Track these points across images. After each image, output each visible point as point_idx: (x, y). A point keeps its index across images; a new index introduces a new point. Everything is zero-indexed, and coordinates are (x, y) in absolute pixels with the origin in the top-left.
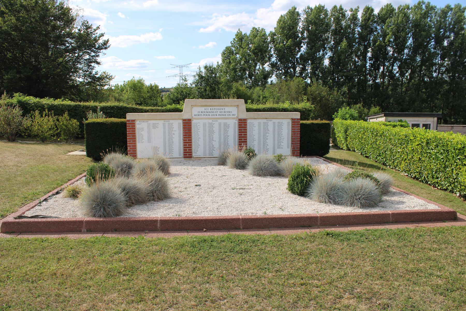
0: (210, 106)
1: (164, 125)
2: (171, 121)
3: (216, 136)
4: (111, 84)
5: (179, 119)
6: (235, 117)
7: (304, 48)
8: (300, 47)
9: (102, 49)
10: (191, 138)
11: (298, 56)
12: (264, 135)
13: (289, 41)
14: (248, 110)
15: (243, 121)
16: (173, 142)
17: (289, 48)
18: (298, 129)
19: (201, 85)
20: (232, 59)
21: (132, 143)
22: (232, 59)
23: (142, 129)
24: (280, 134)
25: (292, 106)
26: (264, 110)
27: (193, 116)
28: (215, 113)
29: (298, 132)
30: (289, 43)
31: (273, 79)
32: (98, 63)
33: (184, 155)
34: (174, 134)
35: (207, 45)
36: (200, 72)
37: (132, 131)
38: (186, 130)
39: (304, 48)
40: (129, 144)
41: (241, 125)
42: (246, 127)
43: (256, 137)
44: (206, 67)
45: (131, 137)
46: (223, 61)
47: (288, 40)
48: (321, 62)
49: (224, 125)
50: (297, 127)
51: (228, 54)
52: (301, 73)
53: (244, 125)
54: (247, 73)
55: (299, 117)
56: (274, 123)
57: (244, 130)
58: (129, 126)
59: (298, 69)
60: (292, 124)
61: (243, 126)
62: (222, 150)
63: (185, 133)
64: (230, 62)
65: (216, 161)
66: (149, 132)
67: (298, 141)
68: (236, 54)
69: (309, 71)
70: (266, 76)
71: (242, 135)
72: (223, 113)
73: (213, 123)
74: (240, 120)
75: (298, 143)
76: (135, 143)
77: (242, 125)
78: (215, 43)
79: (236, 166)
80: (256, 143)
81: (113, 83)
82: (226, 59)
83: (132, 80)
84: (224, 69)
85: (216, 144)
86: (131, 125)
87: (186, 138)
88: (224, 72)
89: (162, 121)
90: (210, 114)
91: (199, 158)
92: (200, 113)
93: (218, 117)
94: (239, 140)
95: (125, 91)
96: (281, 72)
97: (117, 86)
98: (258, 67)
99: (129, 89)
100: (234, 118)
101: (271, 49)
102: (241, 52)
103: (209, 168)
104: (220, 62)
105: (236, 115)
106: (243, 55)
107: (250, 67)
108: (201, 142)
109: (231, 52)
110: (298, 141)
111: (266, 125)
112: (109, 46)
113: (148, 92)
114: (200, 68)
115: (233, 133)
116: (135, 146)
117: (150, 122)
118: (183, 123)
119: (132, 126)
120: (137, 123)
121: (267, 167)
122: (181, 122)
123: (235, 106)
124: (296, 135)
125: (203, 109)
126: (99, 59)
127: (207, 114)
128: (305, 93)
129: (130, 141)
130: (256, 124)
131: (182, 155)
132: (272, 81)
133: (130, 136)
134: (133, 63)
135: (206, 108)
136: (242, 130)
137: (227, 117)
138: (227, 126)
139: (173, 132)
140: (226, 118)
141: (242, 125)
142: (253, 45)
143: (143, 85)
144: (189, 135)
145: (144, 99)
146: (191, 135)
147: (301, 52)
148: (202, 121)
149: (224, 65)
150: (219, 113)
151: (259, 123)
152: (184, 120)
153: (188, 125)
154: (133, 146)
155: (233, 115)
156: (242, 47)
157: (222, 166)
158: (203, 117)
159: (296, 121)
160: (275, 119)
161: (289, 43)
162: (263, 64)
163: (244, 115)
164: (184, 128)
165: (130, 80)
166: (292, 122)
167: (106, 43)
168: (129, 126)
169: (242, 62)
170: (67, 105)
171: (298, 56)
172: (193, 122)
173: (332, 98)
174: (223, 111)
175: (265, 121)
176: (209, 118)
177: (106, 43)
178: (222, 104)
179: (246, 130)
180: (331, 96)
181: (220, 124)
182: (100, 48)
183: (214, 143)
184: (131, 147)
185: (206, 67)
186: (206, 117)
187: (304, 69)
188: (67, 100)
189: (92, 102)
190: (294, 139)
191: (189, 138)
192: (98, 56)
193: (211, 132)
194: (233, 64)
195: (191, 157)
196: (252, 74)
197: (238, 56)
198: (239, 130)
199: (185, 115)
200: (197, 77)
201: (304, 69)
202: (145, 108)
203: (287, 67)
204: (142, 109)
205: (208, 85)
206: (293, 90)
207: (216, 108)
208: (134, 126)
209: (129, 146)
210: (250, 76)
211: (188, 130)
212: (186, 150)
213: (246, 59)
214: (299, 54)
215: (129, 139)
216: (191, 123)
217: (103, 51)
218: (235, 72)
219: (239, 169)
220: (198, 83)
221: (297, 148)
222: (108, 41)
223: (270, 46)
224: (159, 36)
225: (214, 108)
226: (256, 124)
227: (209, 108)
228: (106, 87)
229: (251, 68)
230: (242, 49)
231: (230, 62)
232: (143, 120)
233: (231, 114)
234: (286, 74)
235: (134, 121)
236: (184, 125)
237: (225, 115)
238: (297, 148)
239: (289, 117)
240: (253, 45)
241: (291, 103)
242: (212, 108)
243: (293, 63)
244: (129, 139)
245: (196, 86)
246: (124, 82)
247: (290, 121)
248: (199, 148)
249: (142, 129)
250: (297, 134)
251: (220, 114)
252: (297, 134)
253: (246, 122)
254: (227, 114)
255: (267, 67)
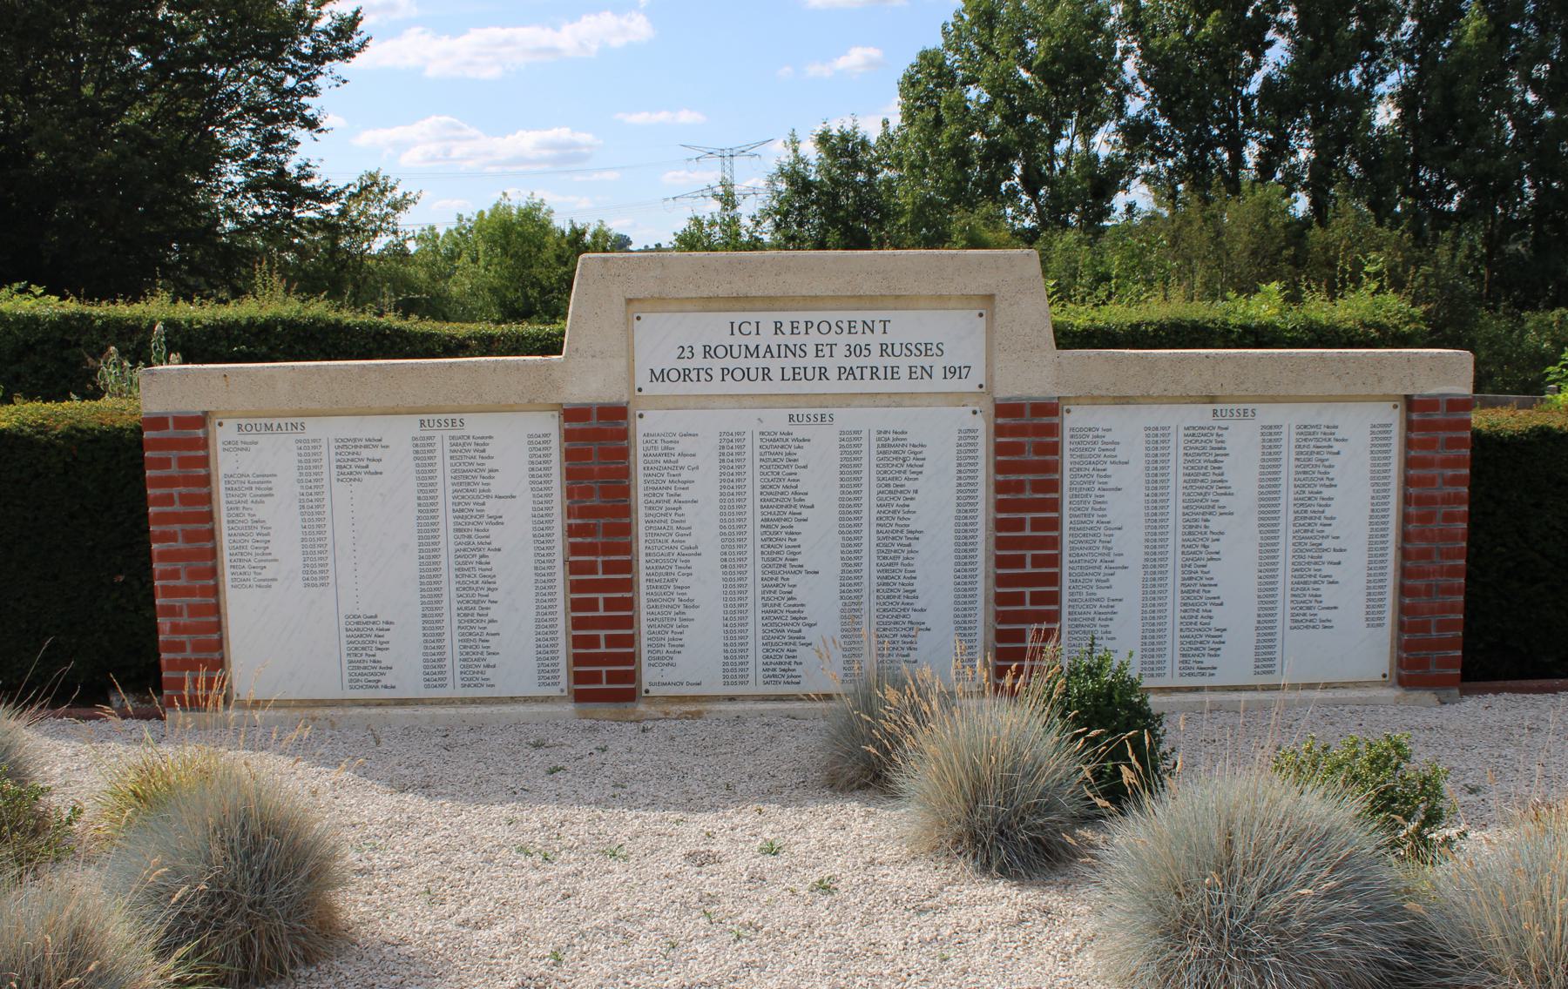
0: (770, 302)
1: (423, 452)
2: (475, 425)
3: (819, 540)
4: (400, 228)
5: (532, 406)
6: (969, 384)
7: (1279, 53)
8: (1260, 48)
9: (330, 57)
10: (627, 548)
11: (1254, 87)
12: (1190, 530)
13: (1210, 20)
14: (1067, 338)
15: (1027, 420)
16: (490, 581)
17: (1210, 49)
18: (1455, 481)
19: (800, 225)
20: (948, 107)
21: (188, 592)
22: (948, 107)
23: (264, 485)
24: (1311, 516)
25: (1294, 318)
26: (1136, 337)
27: (642, 379)
28: (810, 361)
29: (1457, 499)
30: (1208, 29)
31: (1137, 197)
32: (311, 124)
33: (578, 678)
34: (497, 520)
35: (841, 63)
36: (799, 160)
37: (186, 500)
38: (587, 492)
39: (1279, 53)
40: (169, 591)
41: (1018, 449)
42: (1055, 467)
43: (1130, 544)
44: (824, 139)
45: (180, 545)
46: (909, 115)
47: (1205, 15)
48: (1358, 113)
49: (884, 446)
50: (1446, 463)
51: (929, 84)
52: (1266, 168)
53: (1041, 449)
54: (1018, 170)
55: (1463, 386)
56: (1270, 433)
57: (1038, 486)
58: (165, 463)
59: (1251, 152)
60: (1409, 444)
61: (1030, 457)
62: (868, 661)
63: (583, 512)
64: (938, 121)
65: (806, 744)
66: (312, 506)
67: (1453, 572)
68: (964, 84)
69: (1303, 155)
70: (1103, 183)
71: (1019, 525)
72: (875, 359)
73: (799, 431)
74: (1005, 409)
75: (1449, 591)
76: (215, 591)
77: (1026, 449)
78: (874, 53)
79: (975, 838)
80: (1127, 587)
81: (410, 222)
82: (921, 109)
83: (497, 206)
84: (912, 152)
85: (820, 597)
86: (173, 455)
87: (591, 549)
88: (912, 166)
89: (408, 427)
90: (775, 365)
91: (692, 705)
92: (699, 361)
93: (833, 385)
94: (1001, 562)
95: (465, 258)
96: (1170, 163)
97: (429, 237)
98: (1061, 146)
99: (482, 247)
100: (958, 399)
101: (1123, 59)
102: (984, 76)
103: (737, 831)
104: (896, 121)
105: (978, 376)
106: (998, 89)
107: (1029, 139)
108: (705, 585)
109: (945, 77)
110: (1453, 572)
111: (1206, 454)
112: (363, 45)
113: (559, 257)
114: (794, 143)
115: (952, 510)
116: (216, 609)
117: (315, 428)
118: (568, 436)
119: (184, 463)
120: (223, 435)
121: (1305, 934)
122: (550, 426)
123: (966, 299)
124: (1437, 525)
125: (714, 327)
126: (312, 105)
127: (753, 363)
128: (1295, 256)
129: (174, 574)
130: (1129, 447)
131: (563, 681)
132: (1130, 208)
133: (171, 537)
134: (526, 141)
135: (738, 317)
136: (1019, 487)
137: (904, 385)
138: (900, 456)
139: (492, 507)
140: (895, 399)
141: (1026, 449)
142: (1044, 42)
143: (544, 227)
144: (610, 530)
145: (544, 291)
146: (627, 530)
147: (1265, 70)
148: (709, 425)
149: (912, 133)
150: (840, 358)
151: (1157, 437)
152: (572, 414)
153: (606, 454)
154: (195, 611)
155: (952, 372)
156: (991, 52)
157: (854, 809)
158: (716, 387)
159: (1438, 416)
160: (1274, 399)
161: (1208, 29)
162: (1087, 131)
163: (1037, 374)
164: (570, 474)
165: (487, 208)
166: (1410, 426)
167: (346, 28)
168: (165, 463)
169: (996, 120)
170: (18, 319)
171: (1254, 87)
172: (646, 427)
173: (1427, 277)
174: (875, 340)
175: (1199, 415)
176: (767, 401)
177: (346, 28)
178: (867, 288)
179: (1055, 486)
180: (1425, 269)
181: (850, 442)
182: (319, 57)
183: (803, 588)
184: (184, 620)
185: (824, 139)
186: (745, 387)
187: (1276, 151)
188: (39, 291)
189: (165, 297)
190: (1425, 554)
191: (608, 549)
192: (313, 93)
193: (785, 505)
194: (953, 129)
195: (630, 696)
196: (1042, 175)
197: (973, 93)
198: (1000, 487)
199: (583, 374)
200: (782, 186)
201: (1276, 151)
202: (446, 328)
203: (1199, 138)
204: (428, 337)
205: (833, 222)
206: (1241, 244)
207: (816, 316)
208: (205, 462)
209: (171, 611)
210: (1032, 182)
211: (605, 492)
212: (594, 642)
213: (1009, 101)
214: (1258, 78)
215: (166, 556)
216: (624, 435)
217: (338, 66)
218: (965, 163)
219: (1004, 872)
220: (786, 215)
221: (1443, 626)
222: (354, 21)
223: (1120, 44)
224: (639, 27)
225: (801, 317)
226: (1129, 447)
227: (767, 319)
228: (379, 244)
229: (1034, 146)
230: (990, 62)
231: (938, 121)
232: (266, 418)
233: (938, 364)
234: (1197, 172)
235: (201, 420)
236: (569, 455)
237: (893, 373)
238: (1443, 626)
239: (1389, 388)
240: (1044, 42)
241: (1294, 298)
242: (786, 318)
243: (1226, 119)
244: (166, 556)
245: (778, 226)
246: (460, 218)
247: (1393, 418)
248: (690, 626)
249: (264, 485)
250: (1449, 517)
251: (853, 362)
252: (1449, 517)
253: (1053, 430)
254: (904, 363)
255: (1105, 143)
